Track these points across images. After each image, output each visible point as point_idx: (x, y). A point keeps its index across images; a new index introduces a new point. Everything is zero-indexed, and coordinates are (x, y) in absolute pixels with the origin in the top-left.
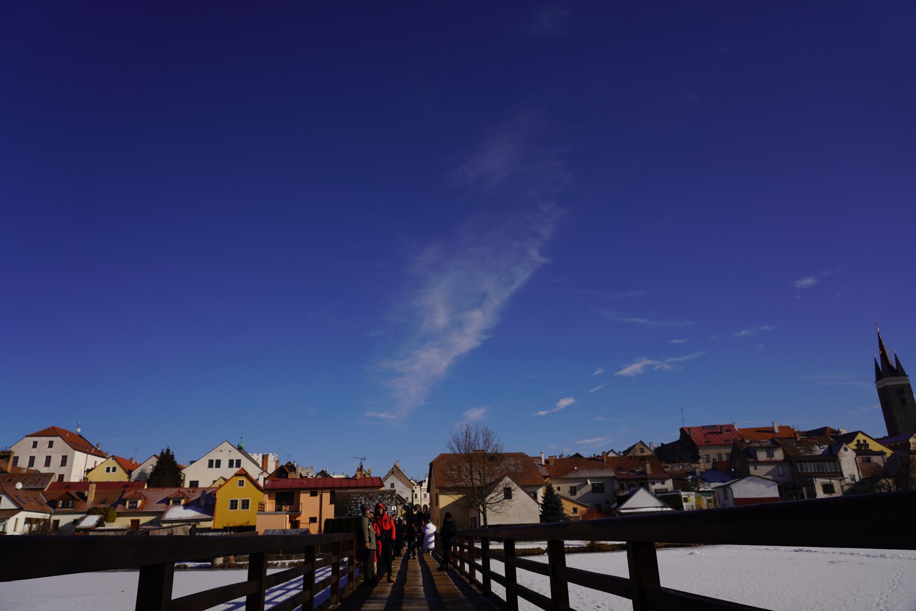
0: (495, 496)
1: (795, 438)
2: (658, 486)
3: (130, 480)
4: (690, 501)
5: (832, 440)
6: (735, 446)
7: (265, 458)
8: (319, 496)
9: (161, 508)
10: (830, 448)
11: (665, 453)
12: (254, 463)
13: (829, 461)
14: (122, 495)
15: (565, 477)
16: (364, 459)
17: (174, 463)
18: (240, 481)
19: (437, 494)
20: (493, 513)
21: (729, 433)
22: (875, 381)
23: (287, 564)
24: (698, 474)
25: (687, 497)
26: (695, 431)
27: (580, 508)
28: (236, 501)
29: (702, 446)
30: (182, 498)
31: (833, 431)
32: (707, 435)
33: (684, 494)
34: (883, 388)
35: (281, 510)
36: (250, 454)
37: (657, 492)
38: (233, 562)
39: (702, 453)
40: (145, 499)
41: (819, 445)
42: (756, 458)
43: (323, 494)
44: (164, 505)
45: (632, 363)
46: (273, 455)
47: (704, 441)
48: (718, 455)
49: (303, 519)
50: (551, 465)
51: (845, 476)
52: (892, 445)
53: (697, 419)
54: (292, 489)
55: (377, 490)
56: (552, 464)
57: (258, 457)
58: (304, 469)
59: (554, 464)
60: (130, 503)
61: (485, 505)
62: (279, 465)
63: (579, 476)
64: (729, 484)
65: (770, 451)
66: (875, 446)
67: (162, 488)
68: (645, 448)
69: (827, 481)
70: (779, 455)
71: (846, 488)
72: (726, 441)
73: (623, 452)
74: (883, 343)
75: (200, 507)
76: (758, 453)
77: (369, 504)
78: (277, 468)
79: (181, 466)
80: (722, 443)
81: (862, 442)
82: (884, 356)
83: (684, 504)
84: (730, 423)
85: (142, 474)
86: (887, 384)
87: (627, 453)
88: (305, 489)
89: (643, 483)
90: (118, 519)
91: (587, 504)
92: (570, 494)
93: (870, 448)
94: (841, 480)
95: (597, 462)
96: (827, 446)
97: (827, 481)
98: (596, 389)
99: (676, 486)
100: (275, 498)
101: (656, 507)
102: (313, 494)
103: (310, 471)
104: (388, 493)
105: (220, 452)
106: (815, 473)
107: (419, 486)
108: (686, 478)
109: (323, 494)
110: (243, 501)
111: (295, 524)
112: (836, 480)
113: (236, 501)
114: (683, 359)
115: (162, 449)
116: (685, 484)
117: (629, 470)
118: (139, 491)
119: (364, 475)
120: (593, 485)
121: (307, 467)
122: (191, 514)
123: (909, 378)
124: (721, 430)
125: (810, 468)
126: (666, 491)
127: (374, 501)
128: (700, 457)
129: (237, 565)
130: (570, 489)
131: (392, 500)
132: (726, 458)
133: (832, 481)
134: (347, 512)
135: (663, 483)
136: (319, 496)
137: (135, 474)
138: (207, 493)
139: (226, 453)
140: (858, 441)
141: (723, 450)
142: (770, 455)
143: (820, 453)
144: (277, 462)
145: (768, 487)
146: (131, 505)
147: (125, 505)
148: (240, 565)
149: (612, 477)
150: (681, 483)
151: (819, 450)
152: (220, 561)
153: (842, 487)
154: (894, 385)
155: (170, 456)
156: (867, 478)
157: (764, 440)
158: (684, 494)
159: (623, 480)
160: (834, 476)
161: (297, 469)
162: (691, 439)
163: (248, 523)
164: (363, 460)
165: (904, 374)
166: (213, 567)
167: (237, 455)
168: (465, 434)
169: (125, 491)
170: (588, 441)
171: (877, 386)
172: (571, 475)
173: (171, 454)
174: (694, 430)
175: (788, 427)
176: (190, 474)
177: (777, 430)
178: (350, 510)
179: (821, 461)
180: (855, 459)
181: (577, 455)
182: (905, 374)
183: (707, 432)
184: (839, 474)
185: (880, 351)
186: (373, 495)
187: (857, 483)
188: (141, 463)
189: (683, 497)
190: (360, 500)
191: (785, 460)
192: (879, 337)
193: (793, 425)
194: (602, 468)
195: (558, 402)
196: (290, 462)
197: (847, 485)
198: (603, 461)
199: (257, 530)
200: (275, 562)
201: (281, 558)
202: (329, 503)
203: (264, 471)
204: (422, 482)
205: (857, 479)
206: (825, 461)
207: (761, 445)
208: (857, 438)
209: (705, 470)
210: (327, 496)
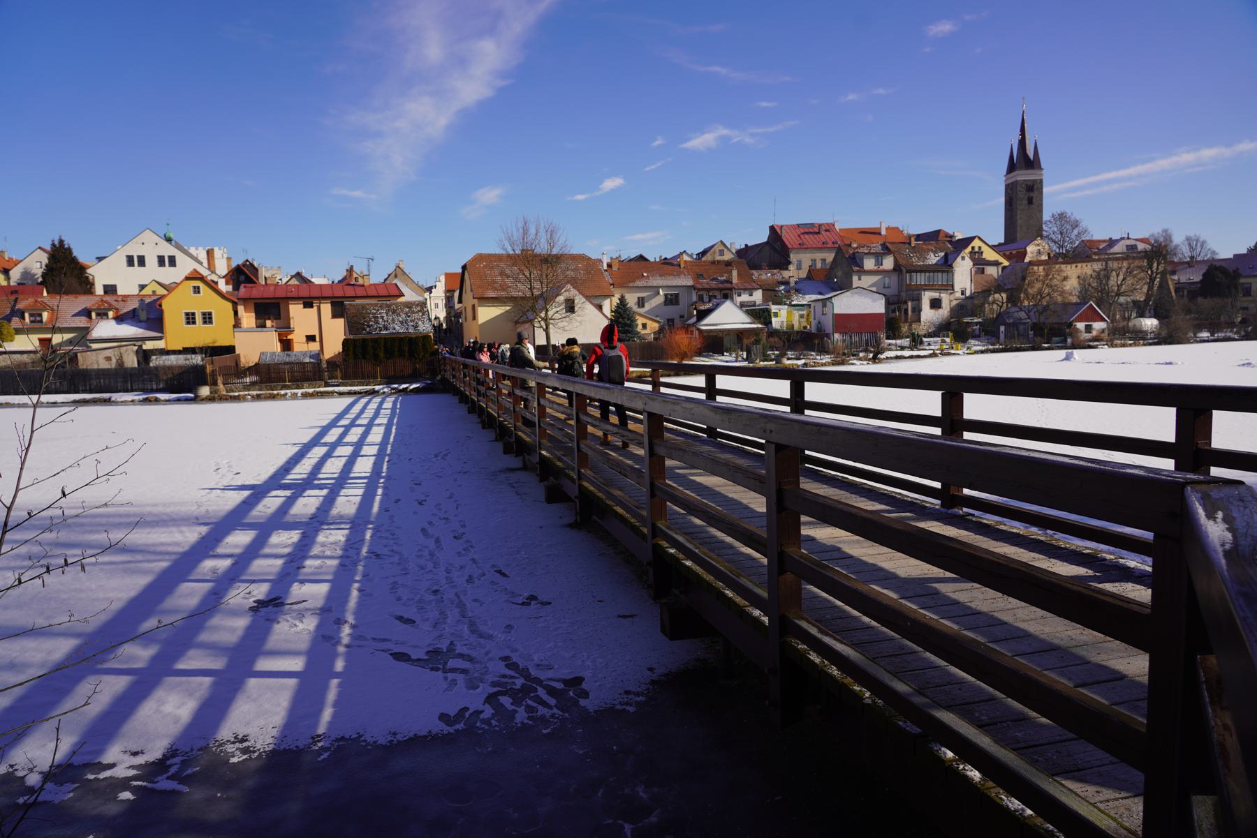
0: (556, 310)
1: (910, 244)
2: (745, 298)
3: (9, 282)
4: (782, 317)
5: (950, 246)
6: (839, 251)
7: (210, 253)
8: (315, 308)
9: (81, 322)
10: (946, 255)
11: (750, 257)
12: (195, 261)
13: (943, 272)
14: (14, 306)
15: (631, 285)
16: (372, 259)
17: (74, 261)
18: (194, 287)
19: (474, 306)
20: (558, 331)
21: (827, 233)
22: (1005, 174)
23: (299, 395)
24: (792, 284)
25: (777, 311)
26: (789, 232)
27: (649, 323)
28: (193, 314)
29: (795, 248)
30: (110, 310)
31: (947, 235)
32: (801, 236)
33: (774, 308)
34: (1012, 183)
35: (264, 326)
36: (186, 248)
37: (742, 305)
38: (224, 393)
39: (793, 257)
40: (52, 310)
41: (935, 252)
42: (862, 267)
43: (321, 305)
44: (83, 319)
45: (703, 133)
46: (220, 249)
47: (797, 243)
48: (812, 260)
49: (298, 338)
50: (613, 269)
51: (956, 290)
52: (1008, 253)
53: (791, 215)
54: (277, 298)
55: (395, 302)
56: (615, 268)
57: (197, 251)
58: (268, 270)
59: (619, 269)
60: (31, 315)
61: (548, 321)
62: (234, 265)
63: (650, 284)
64: (831, 298)
65: (879, 257)
66: (990, 255)
67: (74, 295)
68: (725, 250)
69: (935, 295)
70: (888, 263)
71: (955, 303)
72: (823, 243)
73: (698, 254)
74: (1026, 125)
75: (141, 322)
76: (865, 260)
77: (393, 320)
78: (230, 269)
79: (85, 265)
80: (820, 246)
81: (976, 250)
82: (1022, 143)
83: (774, 320)
84: (829, 221)
85: (27, 274)
86: (1019, 179)
87: (702, 256)
88: (296, 299)
89: (726, 293)
90: (17, 337)
91: (658, 319)
92: (637, 306)
93: (984, 257)
94: (951, 293)
95: (669, 265)
96: (942, 254)
97: (935, 295)
98: (653, 167)
99: (766, 299)
100: (253, 311)
101: (743, 323)
102: (308, 305)
103: (276, 272)
104: (417, 305)
105: (141, 245)
106: (925, 285)
107: (428, 293)
108: (777, 289)
109: (321, 305)
110: (204, 314)
111: (287, 345)
112: (946, 293)
113: (193, 314)
114: (770, 130)
115: (52, 239)
116: (776, 296)
117: (711, 278)
118: (39, 300)
119: (356, 278)
120: (666, 296)
121: (272, 267)
122: (128, 330)
123: (1043, 172)
124: (819, 230)
125: (920, 279)
126: (754, 304)
127: (399, 315)
128: (790, 263)
129: (231, 397)
130: (636, 300)
131: (423, 314)
132: (820, 265)
133: (942, 295)
134: (365, 329)
135: (751, 295)
136: (315, 308)
137: (15, 274)
138: (146, 302)
139: (151, 247)
140: (973, 248)
141: (818, 254)
142: (879, 263)
143: (934, 262)
144: (229, 259)
145: (874, 301)
146: (32, 319)
147: (23, 318)
148: (235, 396)
149: (690, 286)
150: (772, 295)
151: (933, 259)
152: (205, 391)
153: (951, 301)
154: (1025, 180)
155: (66, 249)
156: (978, 292)
157: (874, 245)
158: (774, 308)
159: (704, 289)
160: (944, 290)
161: (260, 270)
162: (782, 240)
163: (214, 342)
164: (370, 260)
165: (1040, 168)
166: (196, 399)
167: (167, 250)
168: (521, 231)
169: (17, 299)
170: (639, 236)
171: (1005, 181)
172: (639, 283)
173: (66, 246)
174: (787, 228)
175: (897, 228)
176: (101, 275)
177: (883, 232)
178: (369, 326)
179: (934, 272)
180: (971, 270)
181: (641, 258)
182: (1040, 167)
183: (803, 231)
184: (950, 287)
185: (1020, 135)
186: (396, 307)
187: (967, 298)
188: (20, 259)
189: (773, 311)
190: (380, 314)
191: (894, 269)
192: (1023, 116)
193: (903, 227)
194: (679, 274)
195: (602, 182)
196: (247, 261)
197: (955, 299)
198: (679, 265)
199: (237, 352)
200: (283, 392)
201: (284, 387)
202: (331, 317)
203: (212, 272)
204: (431, 288)
205: (968, 294)
206: (938, 271)
207: (870, 250)
208: (972, 245)
209: (798, 278)
210: (326, 308)
